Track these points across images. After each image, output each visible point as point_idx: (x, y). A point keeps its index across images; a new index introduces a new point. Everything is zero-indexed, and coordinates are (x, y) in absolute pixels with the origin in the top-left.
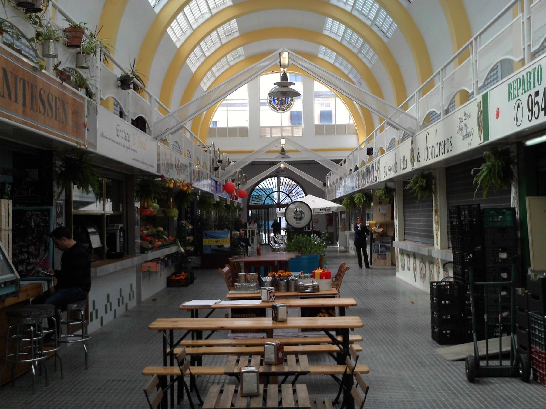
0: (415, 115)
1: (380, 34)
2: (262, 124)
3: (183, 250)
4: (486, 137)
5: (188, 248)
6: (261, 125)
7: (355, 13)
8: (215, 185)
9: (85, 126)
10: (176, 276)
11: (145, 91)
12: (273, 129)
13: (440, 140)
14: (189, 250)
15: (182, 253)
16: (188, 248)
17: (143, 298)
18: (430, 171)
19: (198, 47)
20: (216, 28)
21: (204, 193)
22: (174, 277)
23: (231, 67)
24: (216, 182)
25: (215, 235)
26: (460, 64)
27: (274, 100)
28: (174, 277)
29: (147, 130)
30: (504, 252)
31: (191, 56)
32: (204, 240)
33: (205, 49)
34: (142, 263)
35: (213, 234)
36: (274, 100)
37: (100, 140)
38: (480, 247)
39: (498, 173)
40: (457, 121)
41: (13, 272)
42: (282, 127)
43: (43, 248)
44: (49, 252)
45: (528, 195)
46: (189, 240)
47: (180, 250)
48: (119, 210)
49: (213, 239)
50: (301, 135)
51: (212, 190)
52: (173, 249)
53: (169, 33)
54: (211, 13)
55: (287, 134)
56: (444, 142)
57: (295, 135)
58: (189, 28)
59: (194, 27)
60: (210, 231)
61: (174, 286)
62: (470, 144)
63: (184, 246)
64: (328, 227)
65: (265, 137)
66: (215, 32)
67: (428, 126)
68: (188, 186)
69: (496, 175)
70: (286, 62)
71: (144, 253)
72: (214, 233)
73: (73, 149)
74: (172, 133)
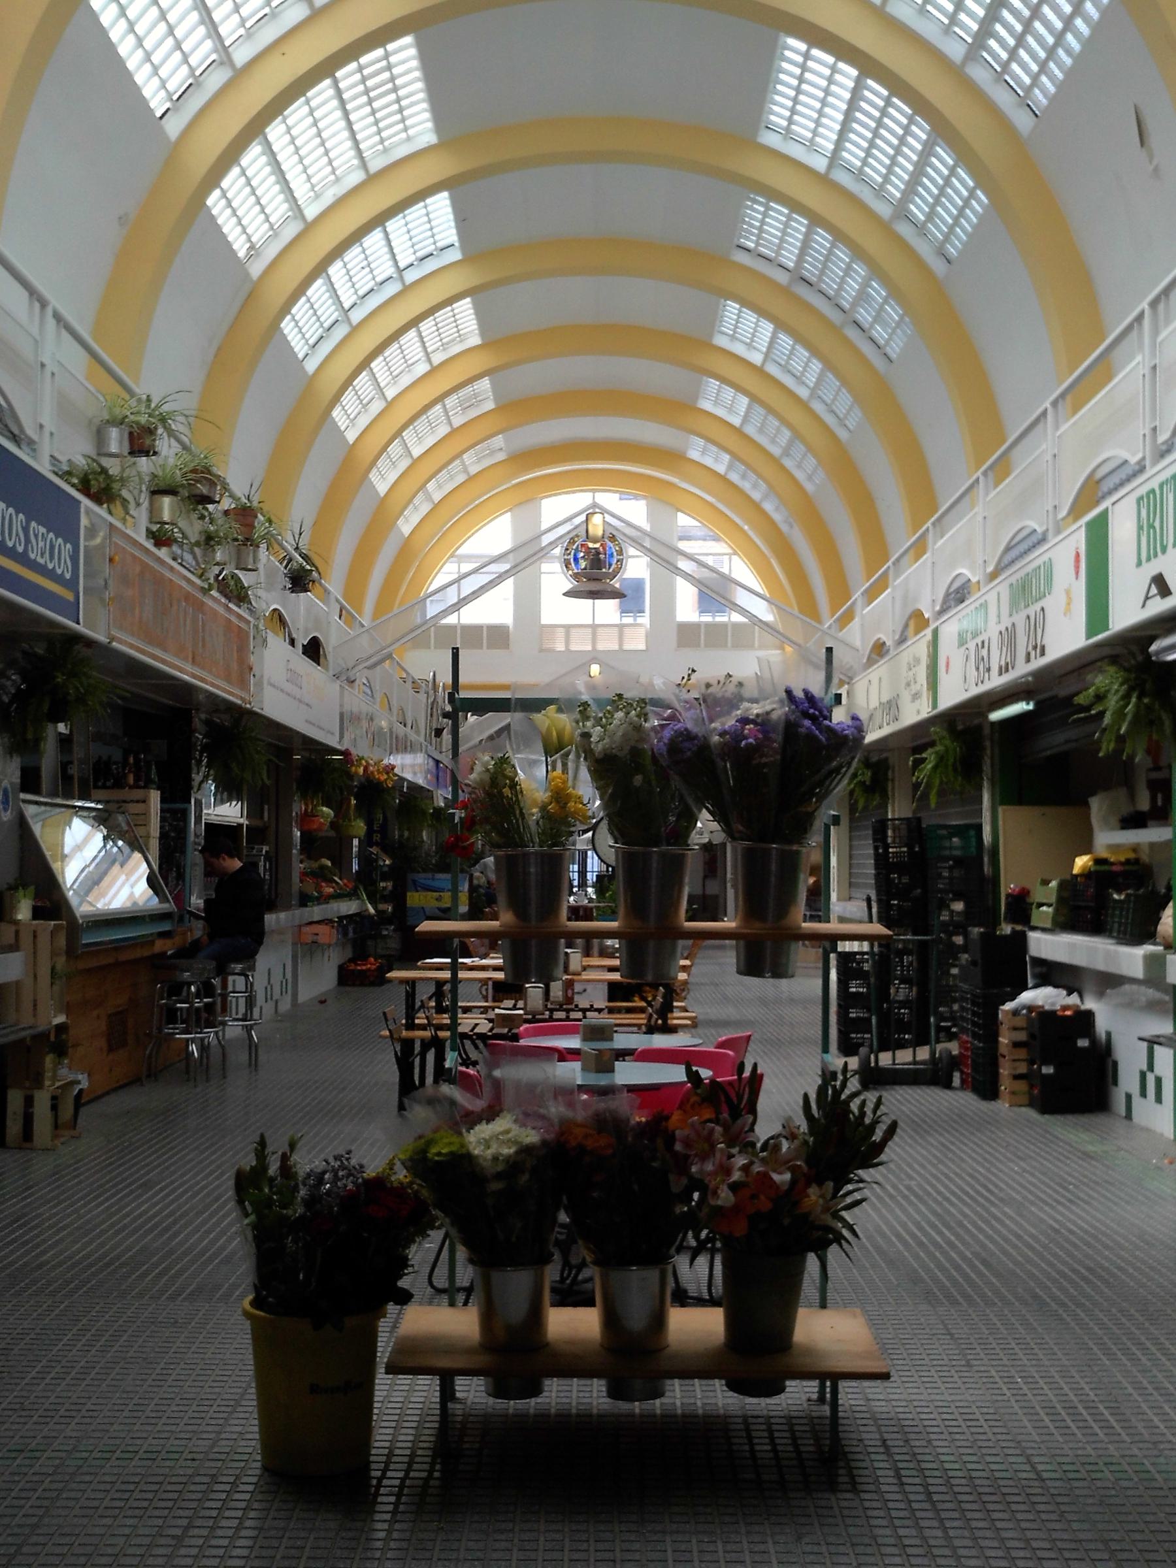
0: (858, 643)
1: (830, 420)
2: (546, 619)
3: (372, 911)
4: (935, 706)
5: (381, 907)
6: (544, 621)
7: (772, 369)
8: (434, 771)
9: (251, 669)
10: (357, 965)
11: (321, 584)
12: (573, 631)
13: (884, 699)
14: (384, 912)
15: (370, 917)
16: (381, 907)
17: (301, 998)
18: (884, 755)
19: (364, 373)
20: (440, 399)
21: (414, 787)
22: (352, 967)
23: (471, 479)
24: (437, 762)
25: (436, 884)
26: (916, 560)
27: (576, 559)
28: (352, 967)
29: (322, 660)
30: (958, 900)
31: (348, 398)
32: (409, 894)
33: (383, 378)
34: (300, 926)
35: (430, 883)
36: (576, 559)
37: (268, 691)
38: (919, 891)
39: (954, 765)
40: (905, 667)
41: (168, 901)
42: (594, 627)
43: (174, 874)
44: (184, 881)
45: (1002, 803)
46: (384, 888)
47: (367, 910)
48: (262, 817)
49: (430, 893)
50: (642, 647)
51: (429, 783)
52: (349, 907)
53: (285, 332)
54: (403, 283)
55: (608, 643)
56: (889, 702)
57: (626, 647)
58: (290, 213)
59: (390, 394)
60: (422, 875)
61: (354, 985)
62: (918, 712)
63: (373, 901)
64: (708, 882)
65: (551, 651)
66: (412, 333)
67: (877, 661)
68: (387, 773)
69: (950, 768)
70: (600, 533)
71: (306, 906)
72: (433, 879)
73: (230, 707)
74: (369, 668)
